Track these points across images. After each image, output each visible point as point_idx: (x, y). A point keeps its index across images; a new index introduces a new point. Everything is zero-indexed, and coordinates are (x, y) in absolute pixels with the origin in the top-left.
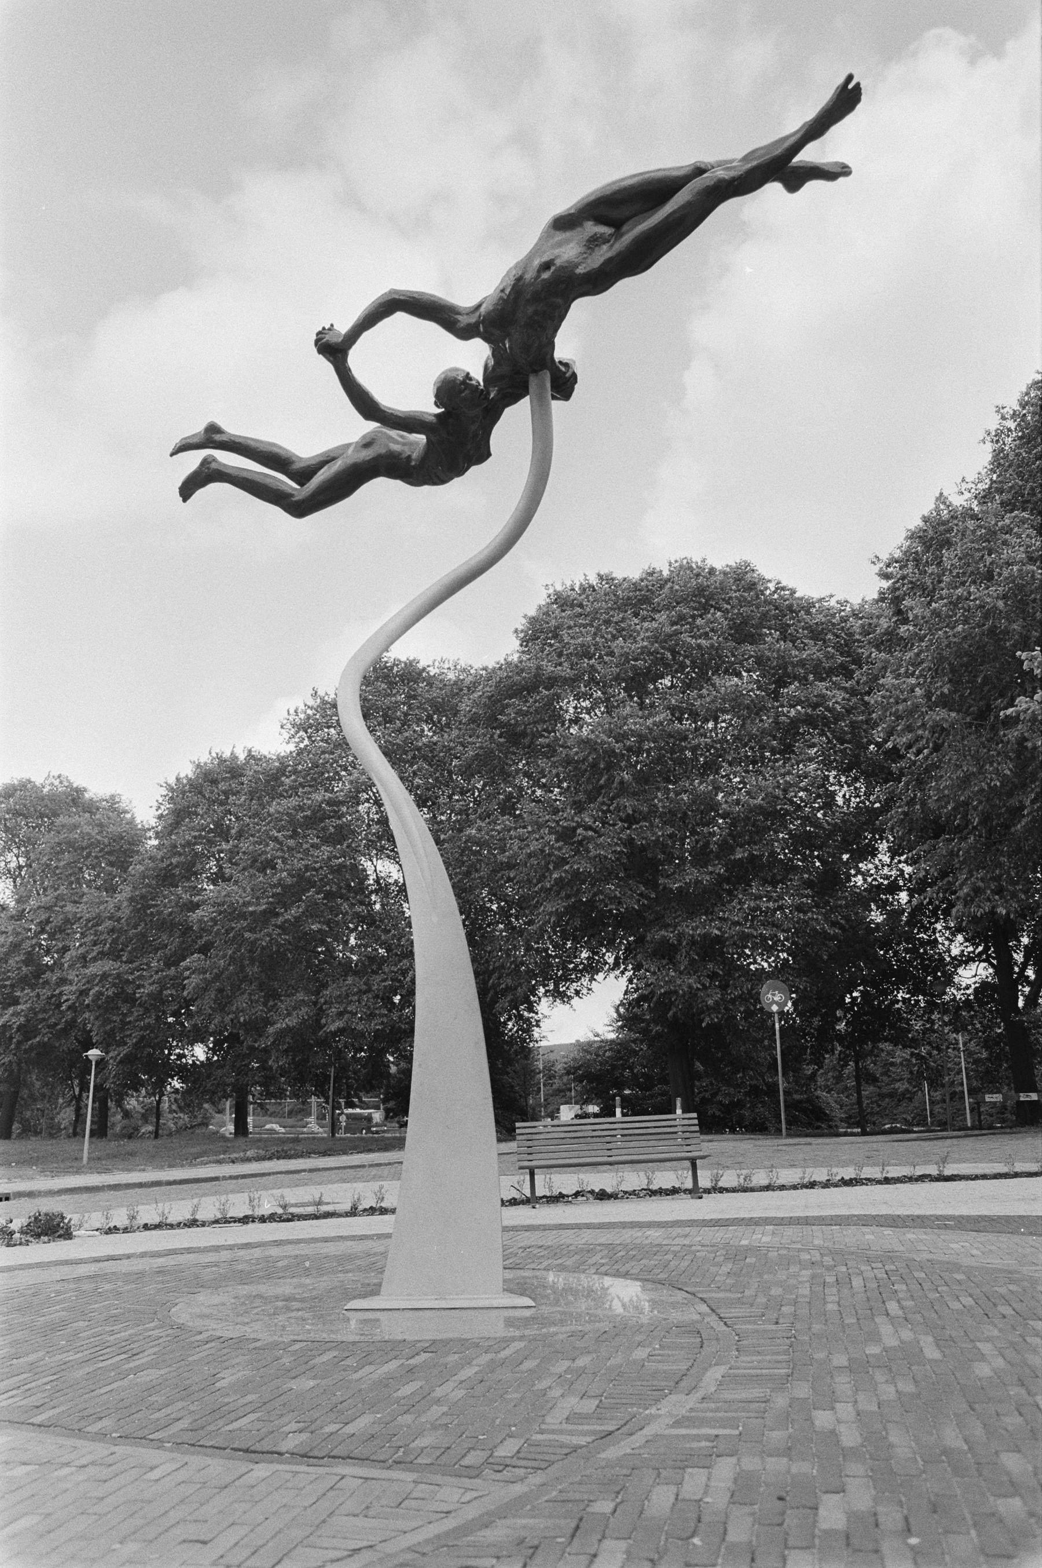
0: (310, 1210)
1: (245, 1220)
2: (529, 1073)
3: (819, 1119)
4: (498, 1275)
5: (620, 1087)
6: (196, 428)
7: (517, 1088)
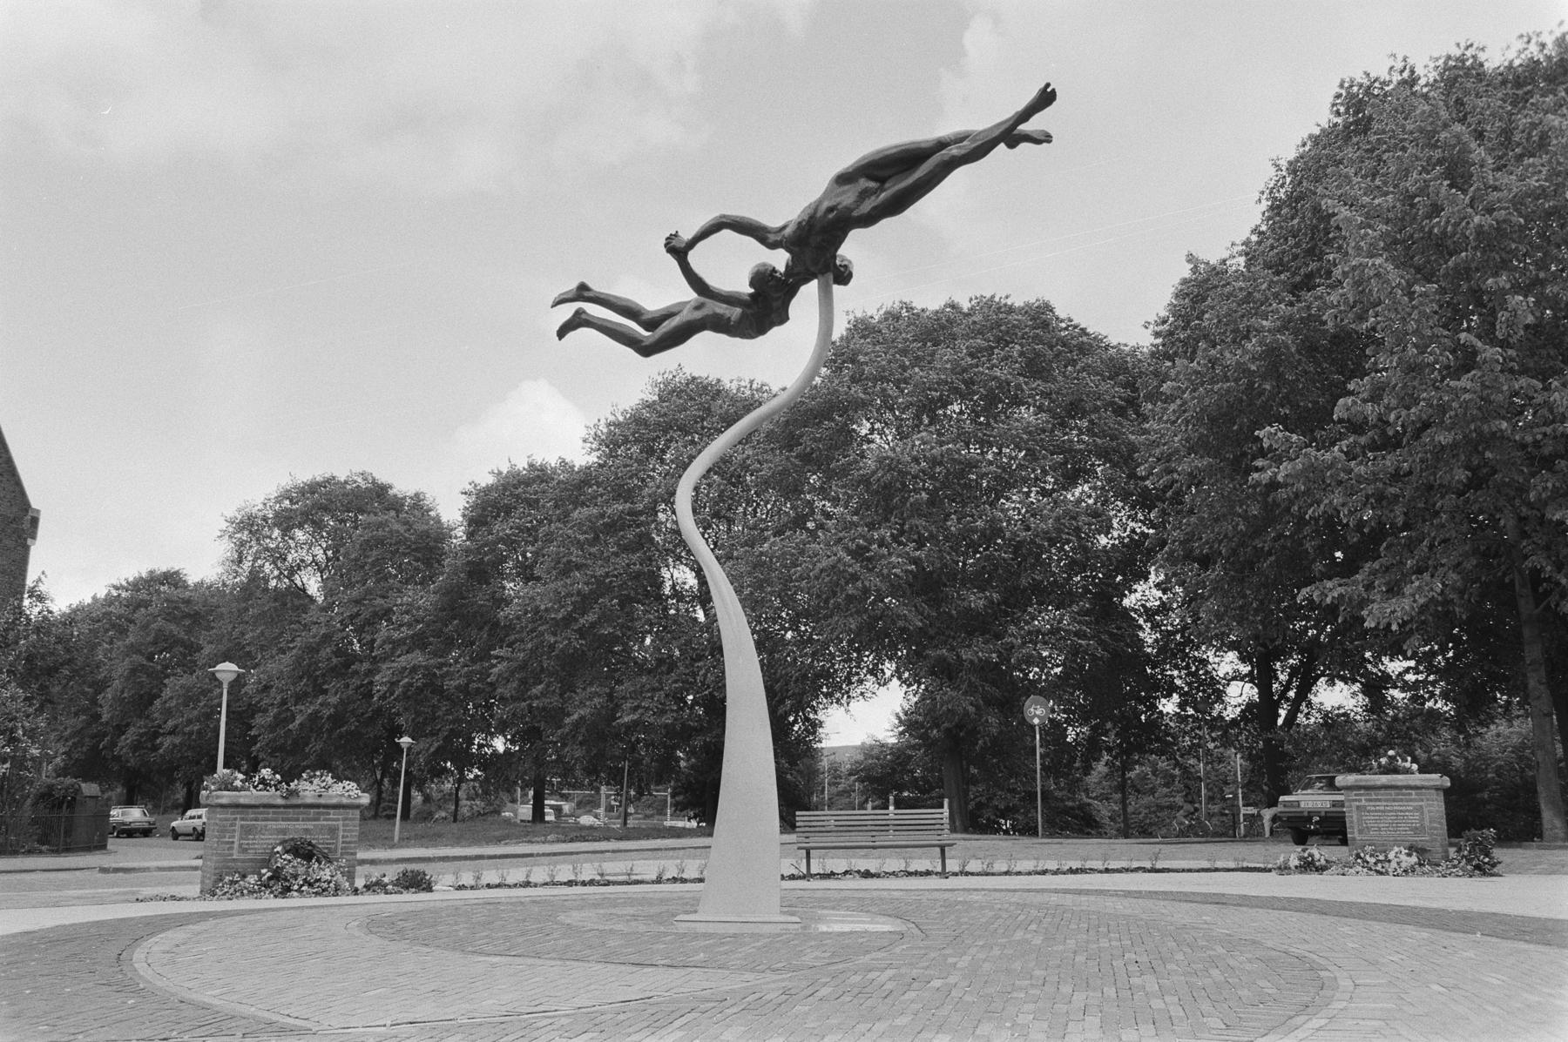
0: (621, 878)
1: (570, 883)
2: (812, 774)
3: (1089, 825)
4: (778, 909)
5: (901, 788)
6: (572, 285)
7: (799, 784)
